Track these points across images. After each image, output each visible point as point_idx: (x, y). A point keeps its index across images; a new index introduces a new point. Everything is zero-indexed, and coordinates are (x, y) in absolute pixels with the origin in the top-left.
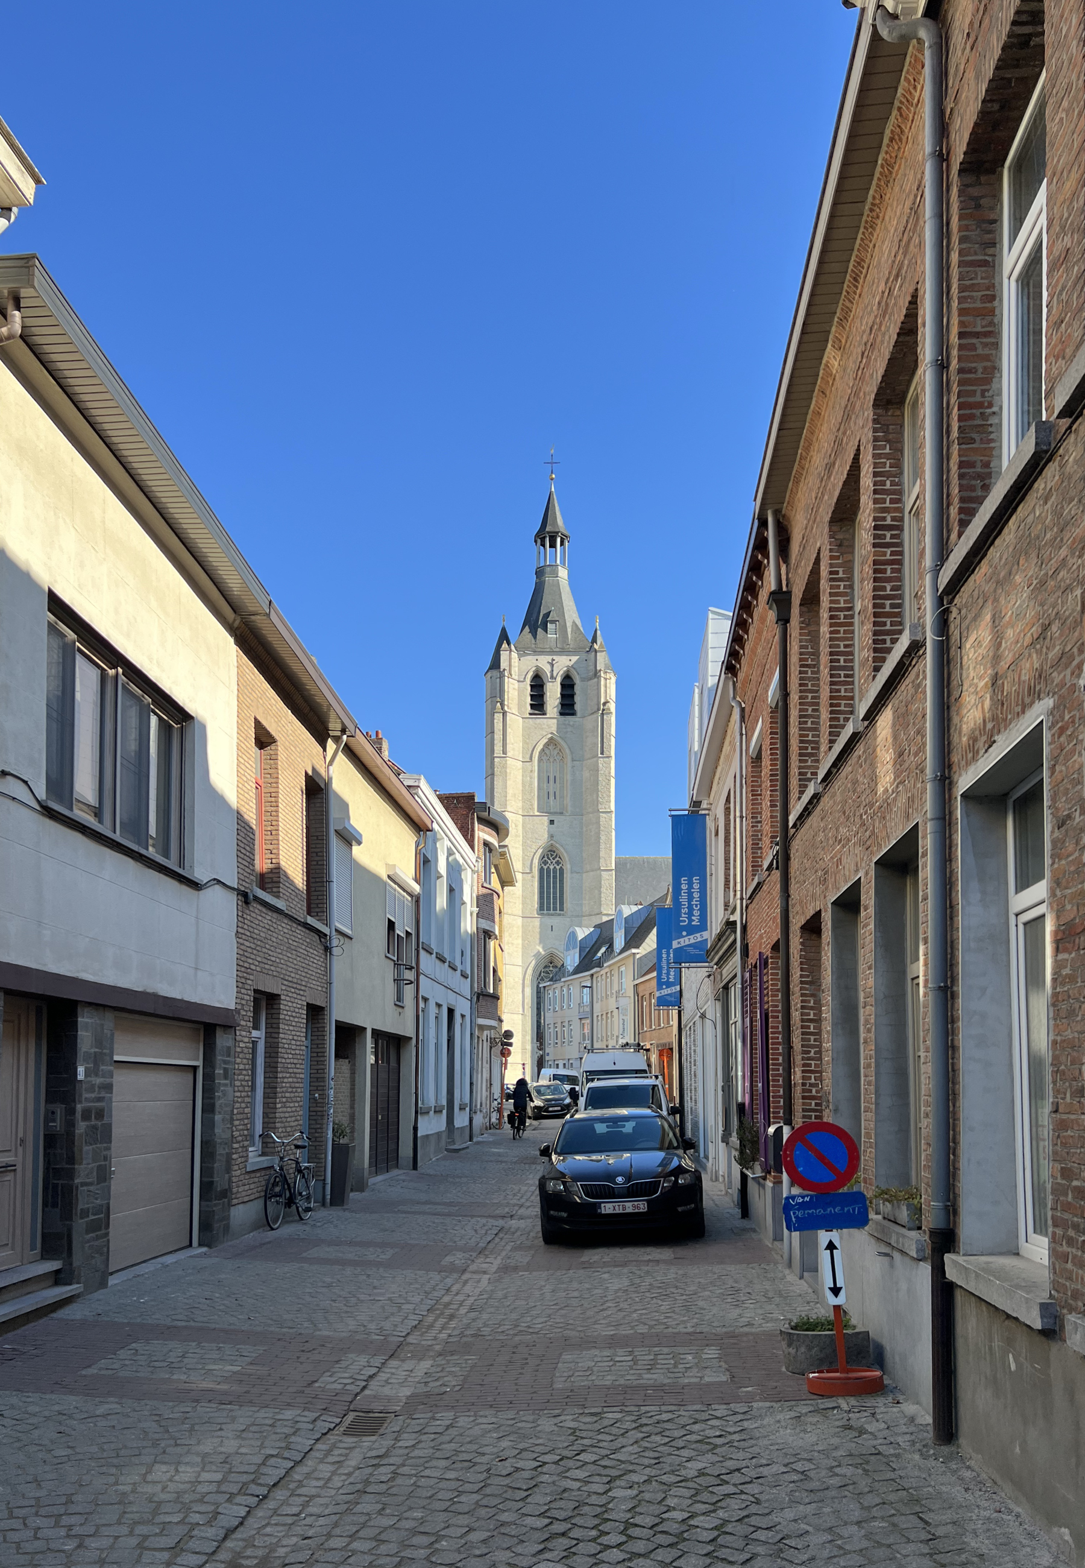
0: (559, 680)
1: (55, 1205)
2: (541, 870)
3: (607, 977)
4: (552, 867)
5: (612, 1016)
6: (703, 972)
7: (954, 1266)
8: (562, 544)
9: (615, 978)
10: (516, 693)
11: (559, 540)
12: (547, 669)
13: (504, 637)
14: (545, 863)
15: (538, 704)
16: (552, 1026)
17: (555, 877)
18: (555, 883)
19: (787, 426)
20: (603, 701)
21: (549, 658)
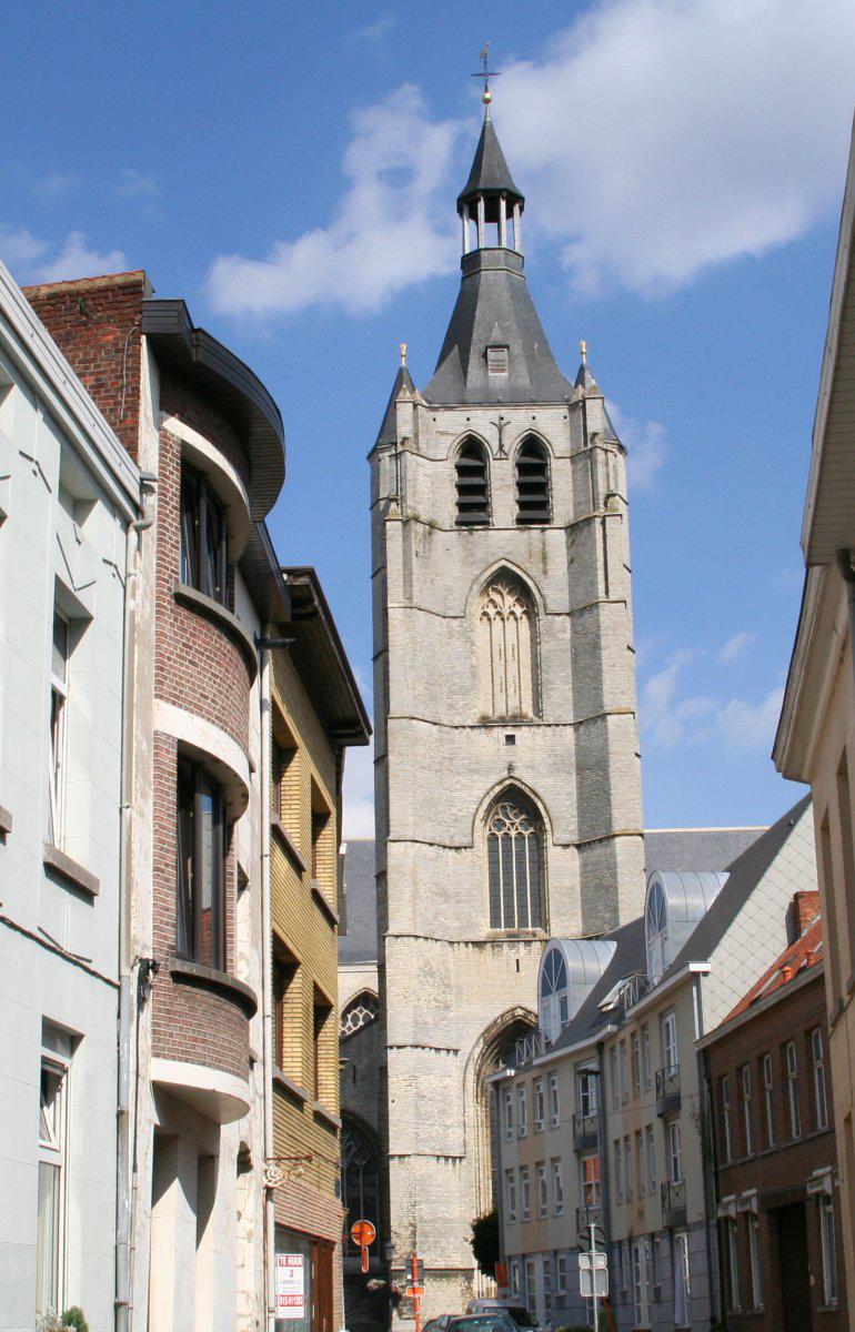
1: (376, 1255)
2: (493, 838)
3: (634, 1045)
4: (513, 833)
5: (651, 1139)
6: (302, 1316)
7: (489, 945)
8: (510, 214)
9: (654, 1043)
10: (431, 484)
11: (503, 204)
12: (488, 435)
13: (401, 379)
16: (516, 1174)
19: (813, 560)
20: (602, 491)
21: (492, 414)
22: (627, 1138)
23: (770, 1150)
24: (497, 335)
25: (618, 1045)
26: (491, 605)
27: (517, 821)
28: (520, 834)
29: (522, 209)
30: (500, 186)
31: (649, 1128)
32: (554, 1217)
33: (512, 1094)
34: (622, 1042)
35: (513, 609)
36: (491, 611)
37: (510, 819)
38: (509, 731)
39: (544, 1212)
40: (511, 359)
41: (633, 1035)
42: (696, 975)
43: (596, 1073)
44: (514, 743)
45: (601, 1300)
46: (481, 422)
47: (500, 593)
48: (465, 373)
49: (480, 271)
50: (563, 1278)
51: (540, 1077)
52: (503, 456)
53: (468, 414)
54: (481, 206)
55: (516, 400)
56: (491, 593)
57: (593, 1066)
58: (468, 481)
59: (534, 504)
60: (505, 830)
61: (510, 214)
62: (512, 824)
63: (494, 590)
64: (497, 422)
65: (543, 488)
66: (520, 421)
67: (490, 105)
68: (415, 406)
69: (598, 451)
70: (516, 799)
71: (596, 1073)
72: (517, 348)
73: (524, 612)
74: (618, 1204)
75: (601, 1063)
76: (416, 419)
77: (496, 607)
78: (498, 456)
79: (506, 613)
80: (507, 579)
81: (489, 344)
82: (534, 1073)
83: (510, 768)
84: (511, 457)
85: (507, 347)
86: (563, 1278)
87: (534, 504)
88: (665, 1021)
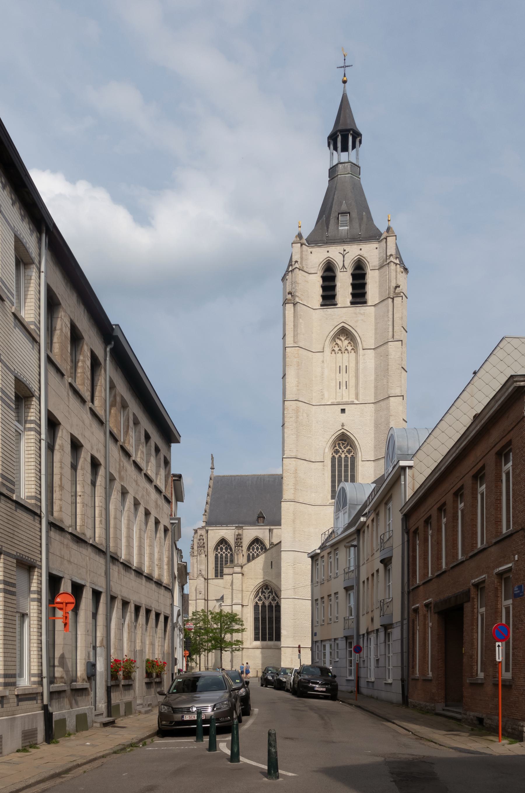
0: (350, 271)
2: (333, 458)
4: (343, 456)
12: (338, 260)
14: (337, 452)
15: (329, 297)
17: (346, 466)
18: (346, 471)
20: (393, 285)
22: (368, 579)
23: (443, 570)
24: (344, 208)
25: (366, 528)
26: (336, 346)
27: (345, 450)
28: (346, 456)
29: (360, 142)
30: (349, 128)
31: (378, 571)
32: (335, 622)
33: (319, 561)
34: (368, 527)
35: (347, 348)
36: (336, 349)
37: (342, 449)
38: (343, 407)
39: (330, 619)
40: (351, 220)
41: (373, 520)
42: (404, 468)
43: (355, 546)
44: (345, 413)
45: (296, 670)
46: (334, 253)
47: (341, 340)
48: (328, 228)
49: (338, 175)
50: (337, 652)
51: (331, 552)
52: (345, 270)
53: (328, 249)
54: (339, 139)
55: (354, 239)
56: (337, 340)
57: (355, 543)
58: (327, 284)
59: (359, 296)
60: (339, 454)
61: (354, 147)
62: (343, 451)
63: (338, 338)
64: (342, 252)
65: (363, 286)
66: (353, 251)
67: (346, 84)
68: (301, 245)
69: (392, 264)
70: (344, 440)
71: (355, 546)
72: (354, 214)
73: (353, 349)
74: (363, 615)
75: (359, 542)
76: (302, 252)
77: (338, 347)
78: (342, 270)
79: (343, 350)
80: (344, 332)
81: (340, 212)
82: (328, 550)
83: (343, 425)
84: (348, 270)
85: (349, 213)
86: (337, 652)
87: (359, 296)
88: (388, 507)
